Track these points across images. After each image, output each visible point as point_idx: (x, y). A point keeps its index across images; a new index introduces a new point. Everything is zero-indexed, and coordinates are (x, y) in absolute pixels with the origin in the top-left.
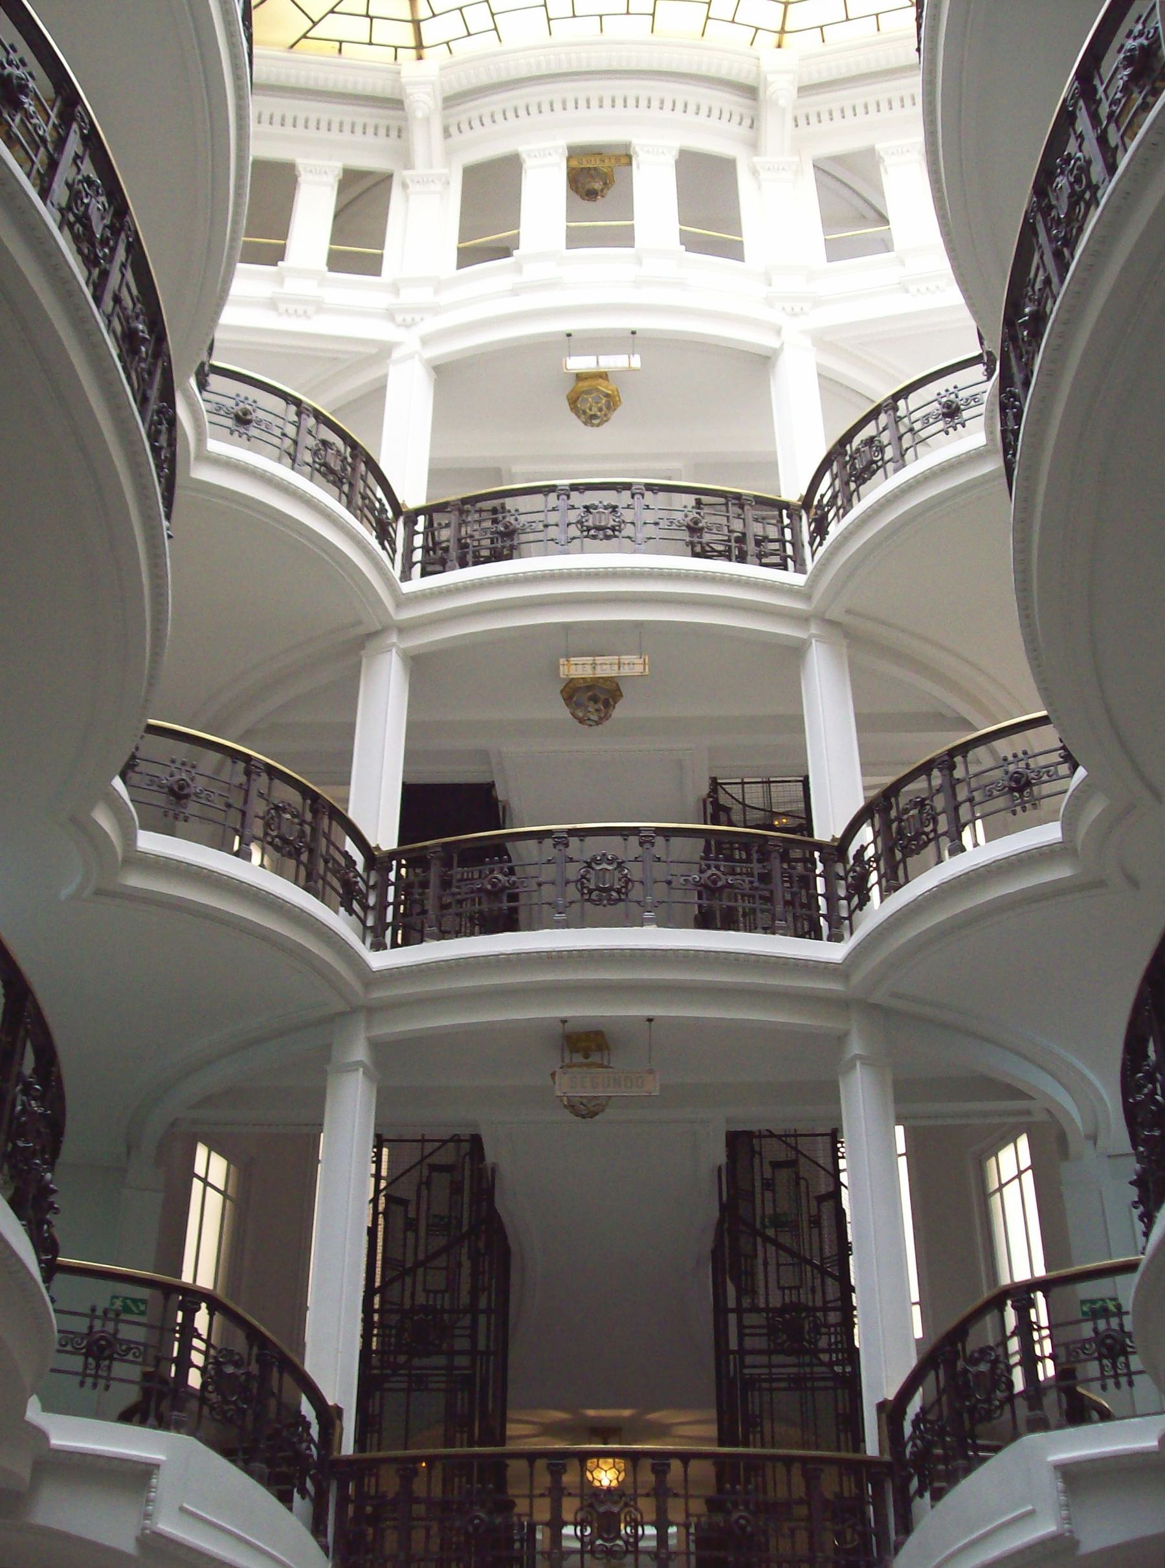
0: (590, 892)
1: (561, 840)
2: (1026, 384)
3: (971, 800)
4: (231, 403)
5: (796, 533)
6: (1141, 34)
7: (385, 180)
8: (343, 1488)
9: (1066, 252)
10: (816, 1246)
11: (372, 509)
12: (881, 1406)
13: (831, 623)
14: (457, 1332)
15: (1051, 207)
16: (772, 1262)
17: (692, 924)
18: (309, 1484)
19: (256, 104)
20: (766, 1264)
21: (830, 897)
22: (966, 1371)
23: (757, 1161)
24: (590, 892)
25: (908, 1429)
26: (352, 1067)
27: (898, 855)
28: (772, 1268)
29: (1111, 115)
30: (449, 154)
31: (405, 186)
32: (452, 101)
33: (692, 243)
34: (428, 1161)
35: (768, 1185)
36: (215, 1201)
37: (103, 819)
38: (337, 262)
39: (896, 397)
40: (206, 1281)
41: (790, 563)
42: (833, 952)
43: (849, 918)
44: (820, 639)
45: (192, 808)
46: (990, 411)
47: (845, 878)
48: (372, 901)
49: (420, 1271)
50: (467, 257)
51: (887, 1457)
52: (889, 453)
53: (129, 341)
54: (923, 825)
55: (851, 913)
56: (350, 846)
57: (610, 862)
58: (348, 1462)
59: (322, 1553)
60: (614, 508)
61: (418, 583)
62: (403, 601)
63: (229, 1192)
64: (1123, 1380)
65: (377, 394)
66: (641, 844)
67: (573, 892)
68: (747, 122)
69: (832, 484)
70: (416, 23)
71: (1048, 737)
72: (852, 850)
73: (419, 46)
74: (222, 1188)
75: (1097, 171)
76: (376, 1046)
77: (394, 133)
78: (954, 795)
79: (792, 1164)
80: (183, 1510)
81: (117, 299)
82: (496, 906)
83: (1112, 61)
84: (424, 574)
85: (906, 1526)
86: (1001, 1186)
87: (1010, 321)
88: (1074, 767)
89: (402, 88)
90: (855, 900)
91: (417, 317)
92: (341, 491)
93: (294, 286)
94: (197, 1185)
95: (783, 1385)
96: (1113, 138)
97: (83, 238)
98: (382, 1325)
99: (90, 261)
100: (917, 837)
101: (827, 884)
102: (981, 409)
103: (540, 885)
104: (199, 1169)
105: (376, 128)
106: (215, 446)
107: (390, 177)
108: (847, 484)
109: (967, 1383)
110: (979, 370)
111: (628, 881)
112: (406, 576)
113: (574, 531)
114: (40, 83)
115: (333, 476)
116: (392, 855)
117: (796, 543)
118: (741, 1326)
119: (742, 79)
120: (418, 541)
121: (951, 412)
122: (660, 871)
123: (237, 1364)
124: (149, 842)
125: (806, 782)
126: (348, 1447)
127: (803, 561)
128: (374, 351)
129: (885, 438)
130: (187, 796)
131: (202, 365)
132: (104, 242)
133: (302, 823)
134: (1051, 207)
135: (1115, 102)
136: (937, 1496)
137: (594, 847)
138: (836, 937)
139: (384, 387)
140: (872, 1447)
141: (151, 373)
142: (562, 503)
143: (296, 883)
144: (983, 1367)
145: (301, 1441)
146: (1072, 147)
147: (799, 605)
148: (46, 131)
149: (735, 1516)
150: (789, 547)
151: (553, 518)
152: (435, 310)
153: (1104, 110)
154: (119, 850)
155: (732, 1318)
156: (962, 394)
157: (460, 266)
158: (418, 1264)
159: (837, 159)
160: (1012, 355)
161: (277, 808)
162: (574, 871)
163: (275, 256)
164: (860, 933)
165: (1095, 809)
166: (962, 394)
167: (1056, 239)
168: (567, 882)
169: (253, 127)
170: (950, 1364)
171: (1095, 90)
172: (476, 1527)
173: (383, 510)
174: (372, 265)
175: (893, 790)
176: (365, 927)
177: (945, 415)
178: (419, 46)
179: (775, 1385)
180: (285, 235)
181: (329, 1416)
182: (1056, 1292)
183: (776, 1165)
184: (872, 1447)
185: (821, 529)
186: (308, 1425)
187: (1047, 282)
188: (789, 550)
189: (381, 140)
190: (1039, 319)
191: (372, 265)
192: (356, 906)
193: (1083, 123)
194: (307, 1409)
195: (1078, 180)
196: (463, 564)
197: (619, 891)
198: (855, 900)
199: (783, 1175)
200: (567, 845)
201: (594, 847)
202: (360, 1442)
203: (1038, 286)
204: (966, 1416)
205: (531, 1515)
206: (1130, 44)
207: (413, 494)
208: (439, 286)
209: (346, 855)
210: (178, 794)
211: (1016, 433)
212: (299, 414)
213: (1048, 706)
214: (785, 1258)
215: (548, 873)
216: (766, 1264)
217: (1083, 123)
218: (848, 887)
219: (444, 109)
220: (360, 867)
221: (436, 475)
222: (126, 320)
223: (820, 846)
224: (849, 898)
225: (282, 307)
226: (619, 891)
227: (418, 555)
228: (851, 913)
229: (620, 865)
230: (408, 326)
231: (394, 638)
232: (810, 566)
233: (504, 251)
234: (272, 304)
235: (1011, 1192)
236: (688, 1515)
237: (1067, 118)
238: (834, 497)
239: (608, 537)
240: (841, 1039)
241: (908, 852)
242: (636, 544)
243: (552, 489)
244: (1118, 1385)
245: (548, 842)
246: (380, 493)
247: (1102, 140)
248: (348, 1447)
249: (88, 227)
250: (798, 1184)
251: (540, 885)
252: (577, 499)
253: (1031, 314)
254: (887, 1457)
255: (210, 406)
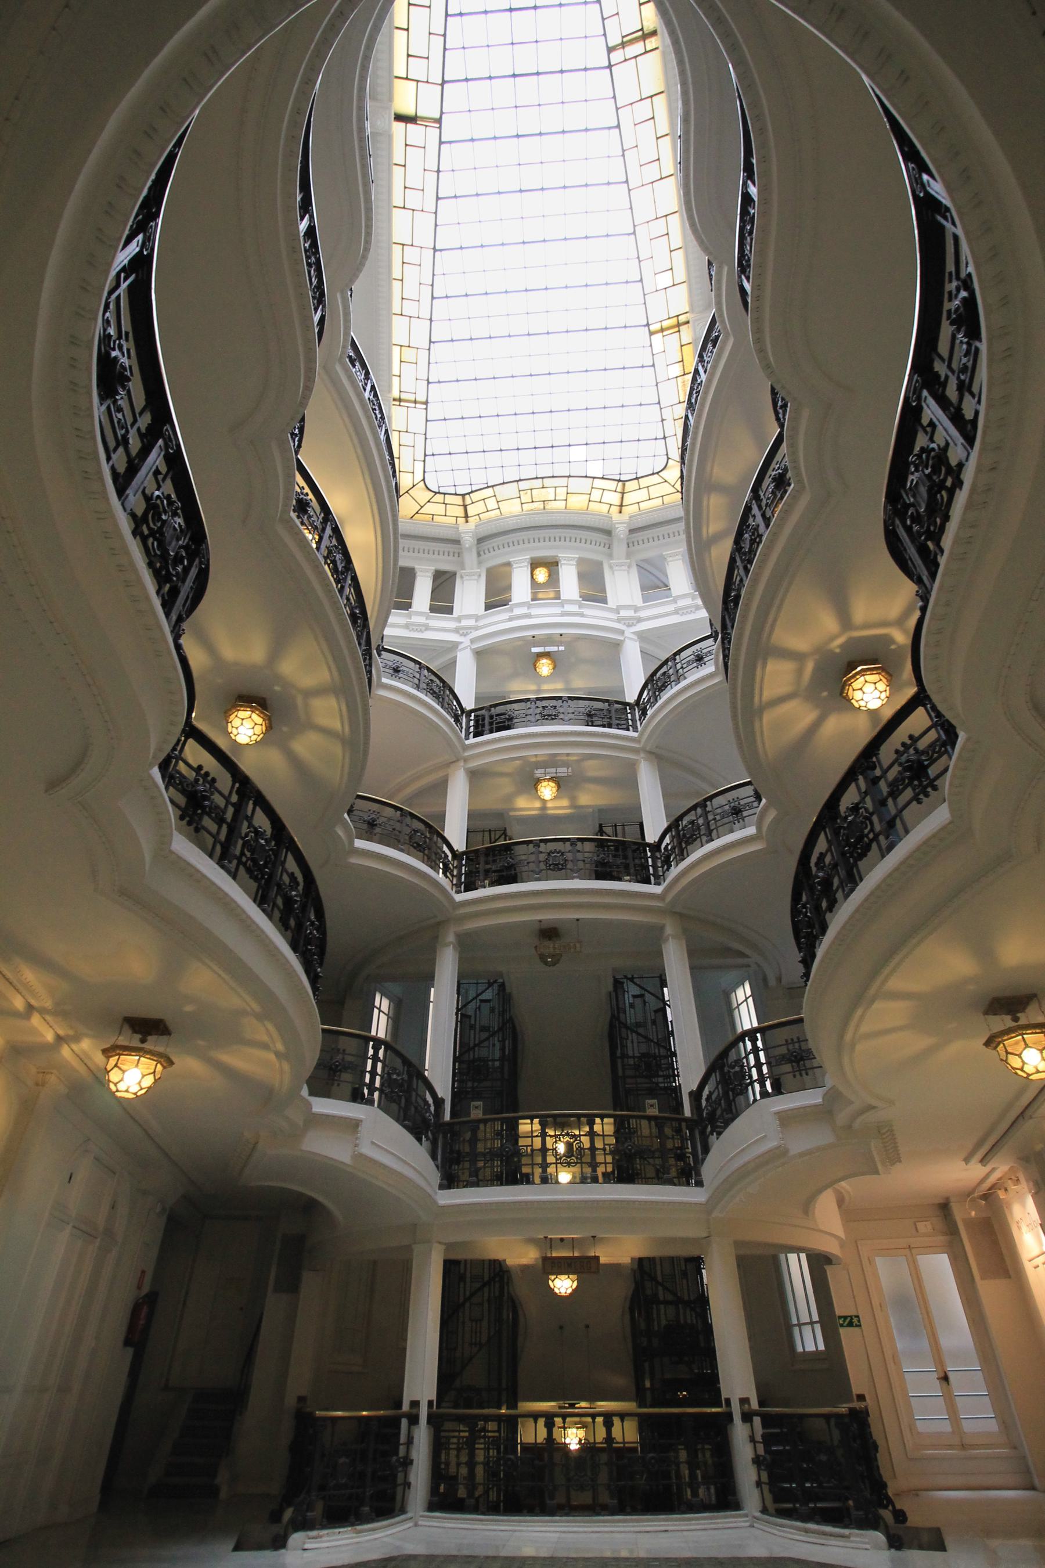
0: (550, 865)
1: (537, 844)
2: (732, 627)
3: (715, 819)
4: (391, 663)
5: (633, 715)
6: (779, 468)
7: (453, 575)
8: (445, 1137)
9: (749, 566)
10: (655, 1034)
11: (452, 709)
12: (691, 1094)
13: (650, 752)
14: (451, 1446)
15: (742, 548)
16: (635, 1041)
17: (594, 876)
18: (430, 1134)
19: (402, 543)
20: (632, 1042)
21: (654, 866)
22: (729, 1072)
23: (626, 996)
24: (550, 865)
25: (704, 1103)
26: (448, 945)
27: (684, 845)
28: (635, 1045)
29: (767, 504)
30: (480, 563)
31: (462, 577)
32: (480, 541)
33: (585, 597)
34: (480, 997)
35: (632, 1006)
36: (384, 1019)
37: (340, 832)
38: (433, 609)
39: (675, 654)
40: (382, 1035)
41: (631, 728)
42: (657, 890)
43: (663, 875)
44: (645, 760)
45: (378, 830)
46: (717, 656)
47: (660, 858)
48: (455, 873)
49: (476, 1048)
50: (488, 607)
51: (695, 1117)
52: (673, 678)
53: (353, 617)
54: (694, 831)
55: (664, 873)
56: (445, 849)
57: (558, 853)
58: (448, 1124)
59: (435, 1168)
60: (555, 707)
61: (472, 740)
62: (466, 748)
63: (390, 1015)
64: (803, 1072)
65: (453, 663)
66: (571, 845)
67: (542, 866)
68: (607, 546)
69: (648, 694)
70: (465, 506)
71: (749, 791)
72: (663, 846)
73: (466, 516)
74: (387, 1012)
75: (762, 528)
76: (458, 936)
77: (456, 555)
78: (707, 818)
79: (642, 996)
80: (373, 1143)
81: (348, 599)
82: (509, 873)
83: (767, 481)
84: (474, 737)
85: (706, 1150)
86: (739, 1005)
87: (725, 602)
88: (760, 800)
89: (460, 534)
90: (666, 867)
91: (469, 631)
92: (424, 854)
93: (415, 619)
94: (376, 1011)
95: (644, 1092)
96: (768, 514)
97: (335, 571)
98: (459, 1072)
99: (337, 581)
100: (691, 836)
101: (652, 861)
102: (713, 656)
103: (528, 863)
104: (377, 1004)
105: (449, 553)
106: (384, 680)
107: (455, 574)
108: (655, 693)
109: (730, 1077)
110: (711, 641)
111: (566, 860)
112: (467, 738)
113: (538, 717)
114: (314, 503)
115: (437, 696)
116: (463, 853)
117: (634, 720)
118: (623, 1066)
119: (605, 528)
120: (472, 723)
121: (699, 659)
122: (580, 856)
123: (398, 1075)
124: (359, 844)
125: (641, 825)
126: (447, 1117)
127: (637, 727)
128: (450, 646)
129: (671, 672)
130: (376, 825)
131: (379, 646)
132: (342, 573)
133: (426, 837)
134: (742, 548)
135: (768, 498)
136: (719, 1134)
137: (551, 846)
138: (658, 884)
139: (456, 661)
140: (687, 1112)
141: (362, 634)
142: (533, 705)
143: (423, 862)
144: (737, 1069)
145: (426, 1112)
146: (751, 521)
147: (637, 745)
148: (318, 524)
149: (626, 1145)
150: (630, 722)
151: (529, 712)
152: (477, 628)
153: (764, 502)
154: (347, 847)
155: (619, 1061)
156: (704, 651)
157: (486, 610)
158: (475, 1045)
159: (644, 561)
160: (727, 617)
161: (414, 830)
162: (542, 857)
163: (407, 606)
164: (667, 881)
165: (772, 814)
166: (704, 651)
167: (745, 560)
168: (540, 862)
169: (401, 553)
170: (722, 1068)
171: (760, 496)
172: (507, 1152)
173: (457, 710)
174: (449, 610)
175: (681, 818)
176: (453, 885)
177: (697, 660)
178: (466, 516)
179: (639, 1092)
180: (411, 597)
181: (439, 1102)
182: (768, 1033)
183: (634, 996)
184: (687, 1112)
185: (644, 713)
186: (429, 1106)
187: (741, 580)
188: (630, 722)
189: (451, 558)
190: (738, 597)
191: (449, 610)
192: (448, 874)
193: (755, 510)
194: (429, 1098)
195: (753, 534)
196: (491, 732)
197: (562, 865)
198: (666, 867)
199: (638, 1001)
200: (539, 846)
201: (551, 846)
202: (453, 1114)
203: (737, 582)
204: (731, 1093)
205: (532, 1146)
206: (774, 473)
207: (469, 704)
208: (477, 618)
209: (444, 852)
210: (372, 824)
211: (729, 649)
212: (420, 668)
213: (751, 775)
214: (641, 1039)
215: (532, 858)
216: (632, 1042)
217: (755, 510)
218: (662, 862)
219: (478, 544)
220: (450, 858)
221: (477, 699)
222: (352, 609)
223: (649, 845)
224: (662, 867)
225: (411, 628)
226: (562, 865)
227: (472, 729)
228: (664, 873)
229: (563, 854)
230: (465, 635)
231: (462, 763)
232: (639, 728)
233: (505, 603)
234: (407, 626)
235: (743, 1007)
236: (605, 1145)
237: (748, 509)
238: (649, 699)
239: (553, 719)
240: (662, 928)
241: (688, 843)
242: (563, 722)
243: (528, 700)
244: (801, 1075)
245: (531, 845)
246: (455, 703)
247: (763, 515)
248: (447, 1117)
249: (335, 565)
250: (645, 1005)
251: (528, 863)
252: (540, 704)
253: (735, 596)
254: (695, 1117)
255: (383, 665)
